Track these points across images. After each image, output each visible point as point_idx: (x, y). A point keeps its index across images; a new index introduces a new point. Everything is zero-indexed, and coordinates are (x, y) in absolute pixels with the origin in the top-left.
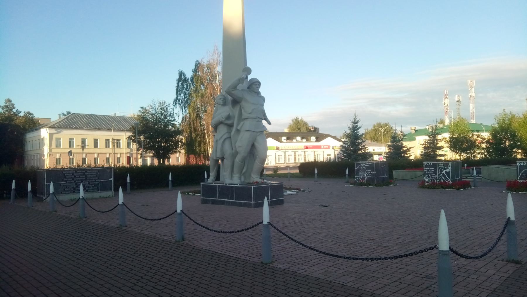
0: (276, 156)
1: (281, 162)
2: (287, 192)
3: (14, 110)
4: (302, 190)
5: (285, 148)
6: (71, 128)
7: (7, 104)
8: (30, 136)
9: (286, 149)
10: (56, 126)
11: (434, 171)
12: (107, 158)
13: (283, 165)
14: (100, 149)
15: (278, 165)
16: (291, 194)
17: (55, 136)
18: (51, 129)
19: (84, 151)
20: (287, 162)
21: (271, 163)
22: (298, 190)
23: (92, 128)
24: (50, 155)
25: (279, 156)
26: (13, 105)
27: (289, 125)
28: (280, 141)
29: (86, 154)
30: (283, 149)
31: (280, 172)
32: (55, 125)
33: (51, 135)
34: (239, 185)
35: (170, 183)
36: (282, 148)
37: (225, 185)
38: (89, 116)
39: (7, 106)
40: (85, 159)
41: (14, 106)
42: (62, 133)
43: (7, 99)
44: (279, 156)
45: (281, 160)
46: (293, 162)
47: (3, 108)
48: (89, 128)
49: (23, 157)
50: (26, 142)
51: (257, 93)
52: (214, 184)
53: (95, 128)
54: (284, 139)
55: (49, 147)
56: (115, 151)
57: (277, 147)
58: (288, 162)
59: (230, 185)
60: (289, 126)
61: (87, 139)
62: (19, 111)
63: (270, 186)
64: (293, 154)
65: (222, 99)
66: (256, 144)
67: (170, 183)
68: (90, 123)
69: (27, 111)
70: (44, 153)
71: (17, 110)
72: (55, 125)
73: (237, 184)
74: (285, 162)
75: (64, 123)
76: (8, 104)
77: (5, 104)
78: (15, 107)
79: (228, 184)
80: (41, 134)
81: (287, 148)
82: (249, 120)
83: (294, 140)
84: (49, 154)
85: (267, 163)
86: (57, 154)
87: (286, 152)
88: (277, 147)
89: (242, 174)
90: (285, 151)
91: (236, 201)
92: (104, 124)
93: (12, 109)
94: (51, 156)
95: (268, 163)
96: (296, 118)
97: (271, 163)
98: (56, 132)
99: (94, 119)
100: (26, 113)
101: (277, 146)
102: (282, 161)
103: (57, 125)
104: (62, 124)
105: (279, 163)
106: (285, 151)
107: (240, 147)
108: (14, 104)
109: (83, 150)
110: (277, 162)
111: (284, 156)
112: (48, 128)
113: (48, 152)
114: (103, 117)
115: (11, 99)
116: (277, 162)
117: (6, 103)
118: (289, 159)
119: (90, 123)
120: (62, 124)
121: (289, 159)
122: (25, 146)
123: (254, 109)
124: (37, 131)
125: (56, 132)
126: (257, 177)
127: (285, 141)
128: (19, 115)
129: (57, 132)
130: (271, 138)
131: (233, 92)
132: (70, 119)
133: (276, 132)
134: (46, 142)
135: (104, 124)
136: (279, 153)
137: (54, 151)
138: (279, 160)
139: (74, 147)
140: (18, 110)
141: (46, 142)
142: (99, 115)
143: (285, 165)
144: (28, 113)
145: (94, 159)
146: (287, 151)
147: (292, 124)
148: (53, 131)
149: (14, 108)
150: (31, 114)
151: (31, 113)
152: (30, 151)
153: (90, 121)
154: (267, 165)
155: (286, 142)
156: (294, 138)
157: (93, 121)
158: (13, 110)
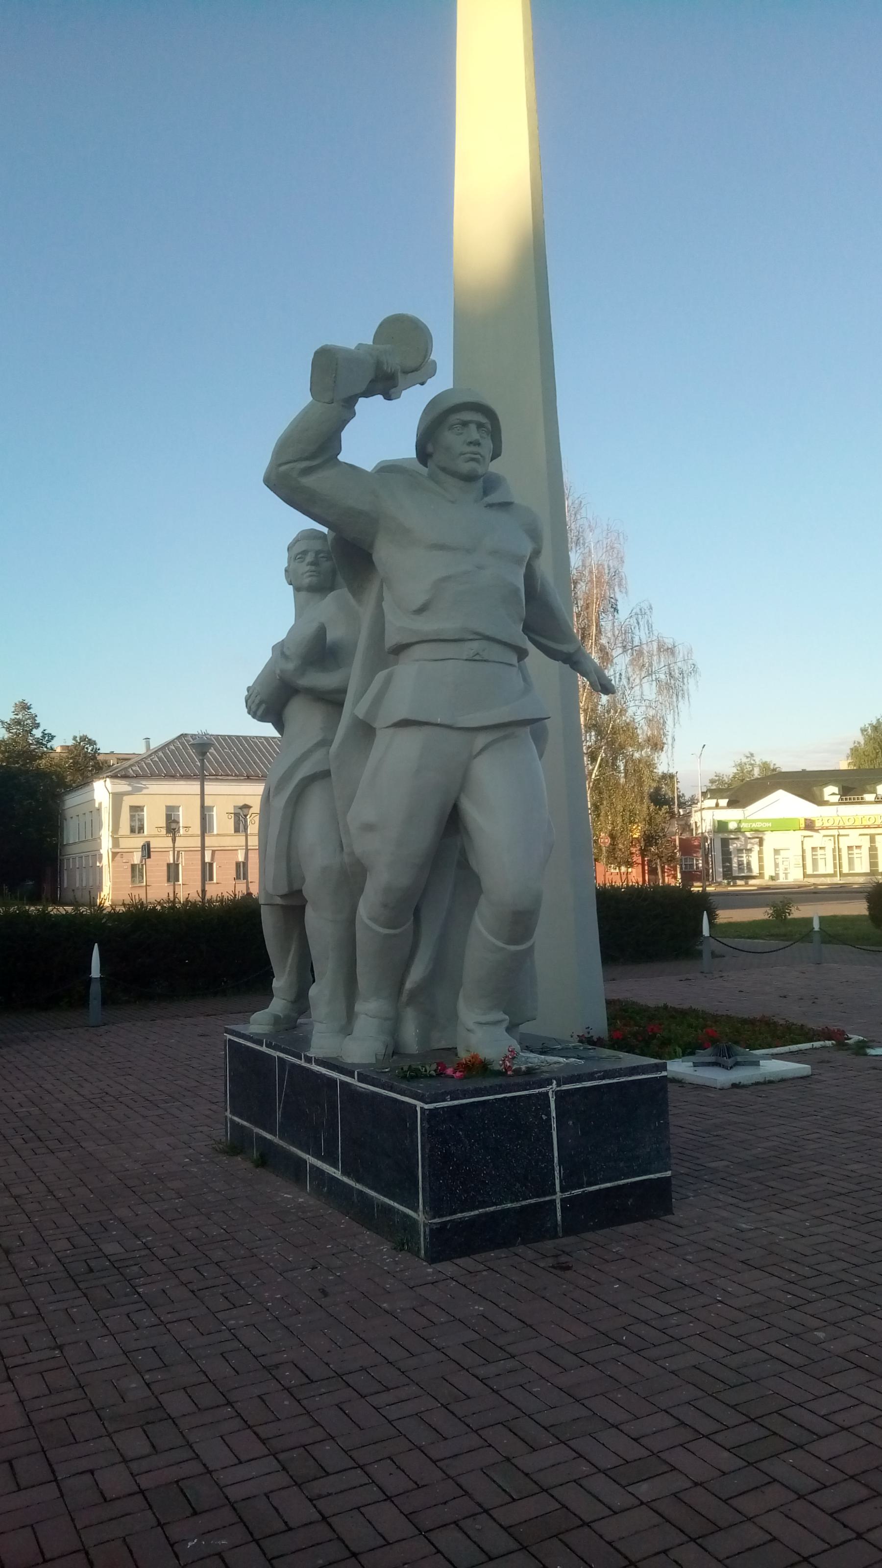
0: (803, 851)
1: (821, 870)
2: (756, 1064)
3: (37, 733)
4: (855, 1038)
5: (836, 824)
6: (171, 776)
7: (17, 717)
8: (72, 801)
9: (839, 828)
10: (131, 771)
11: (593, 733)
12: (238, 864)
13: (829, 880)
14: (218, 835)
15: (812, 881)
16: (783, 1080)
17: (128, 802)
18: (116, 781)
19: (176, 845)
20: (845, 870)
21: (786, 874)
22: (828, 1043)
23: (228, 775)
24: (115, 854)
25: (814, 849)
26: (34, 718)
27: (852, 746)
28: (819, 801)
29: (213, 852)
30: (827, 828)
31: (798, 912)
32: (130, 770)
33: (117, 798)
34: (362, 1078)
35: (95, 990)
36: (826, 824)
37: (303, 1063)
38: (224, 740)
39: (18, 722)
40: (211, 865)
41: (35, 720)
42: (145, 791)
43: (19, 702)
44: (814, 849)
45: (821, 863)
46: (866, 869)
47: (8, 729)
48: (221, 775)
49: (59, 861)
50: (66, 820)
51: (480, 483)
52: (264, 1049)
53: (237, 776)
54: (830, 792)
55: (112, 832)
56: (207, 844)
57: (806, 820)
58: (850, 870)
59: (323, 1070)
60: (852, 749)
61: (215, 809)
62: (49, 734)
63: (557, 1093)
64: (865, 843)
65: (310, 558)
66: (471, 811)
67: (95, 990)
68: (225, 761)
69: (82, 735)
70: (102, 851)
71: (43, 732)
72: (130, 770)
73: (351, 1074)
74: (835, 872)
75: (155, 762)
76: (20, 716)
77: (13, 717)
78: (39, 724)
79: (320, 1062)
80: (95, 797)
81: (841, 824)
82: (418, 651)
83: (870, 797)
84: (113, 853)
85: (773, 874)
86: (239, 851)
87: (838, 835)
88: (806, 820)
89: (404, 998)
90: (835, 832)
91: (345, 1179)
92: (263, 763)
93: (31, 730)
94: (116, 858)
95: (777, 875)
96: (874, 722)
97: (786, 874)
98: (129, 788)
99: (239, 749)
100: (78, 739)
101: (806, 817)
102: (826, 867)
103: (134, 768)
104: (148, 765)
105: (815, 873)
106: (835, 832)
107: (369, 828)
108: (36, 716)
109: (174, 841)
110: (809, 871)
111: (834, 850)
112: (108, 779)
113: (111, 846)
114: (262, 743)
115: (28, 701)
116: (809, 871)
117: (17, 714)
118: (851, 861)
119: (225, 761)
120: (148, 765)
121: (851, 861)
122: (62, 831)
123: (445, 579)
124: (87, 789)
125: (129, 788)
126: (496, 1023)
127: (836, 798)
128: (49, 745)
129: (133, 787)
130: (786, 790)
131: (309, 481)
132: (172, 752)
133: (804, 771)
134: (106, 817)
135: (263, 763)
136: (817, 839)
137: (125, 843)
138: (815, 862)
139: (213, 832)
140: (46, 732)
141: (106, 817)
142: (253, 737)
143: (837, 880)
144: (84, 738)
145: (165, 868)
146: (842, 832)
147: (862, 742)
148: (123, 786)
149: (37, 726)
150: (92, 742)
151: (90, 740)
152: (75, 843)
153: (227, 753)
154: (771, 883)
155: (840, 804)
156: (868, 787)
157: (234, 754)
158: (34, 732)
